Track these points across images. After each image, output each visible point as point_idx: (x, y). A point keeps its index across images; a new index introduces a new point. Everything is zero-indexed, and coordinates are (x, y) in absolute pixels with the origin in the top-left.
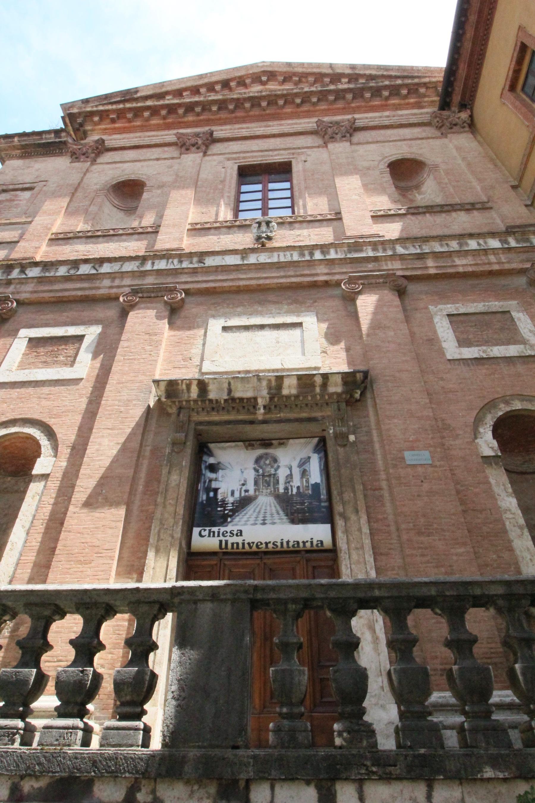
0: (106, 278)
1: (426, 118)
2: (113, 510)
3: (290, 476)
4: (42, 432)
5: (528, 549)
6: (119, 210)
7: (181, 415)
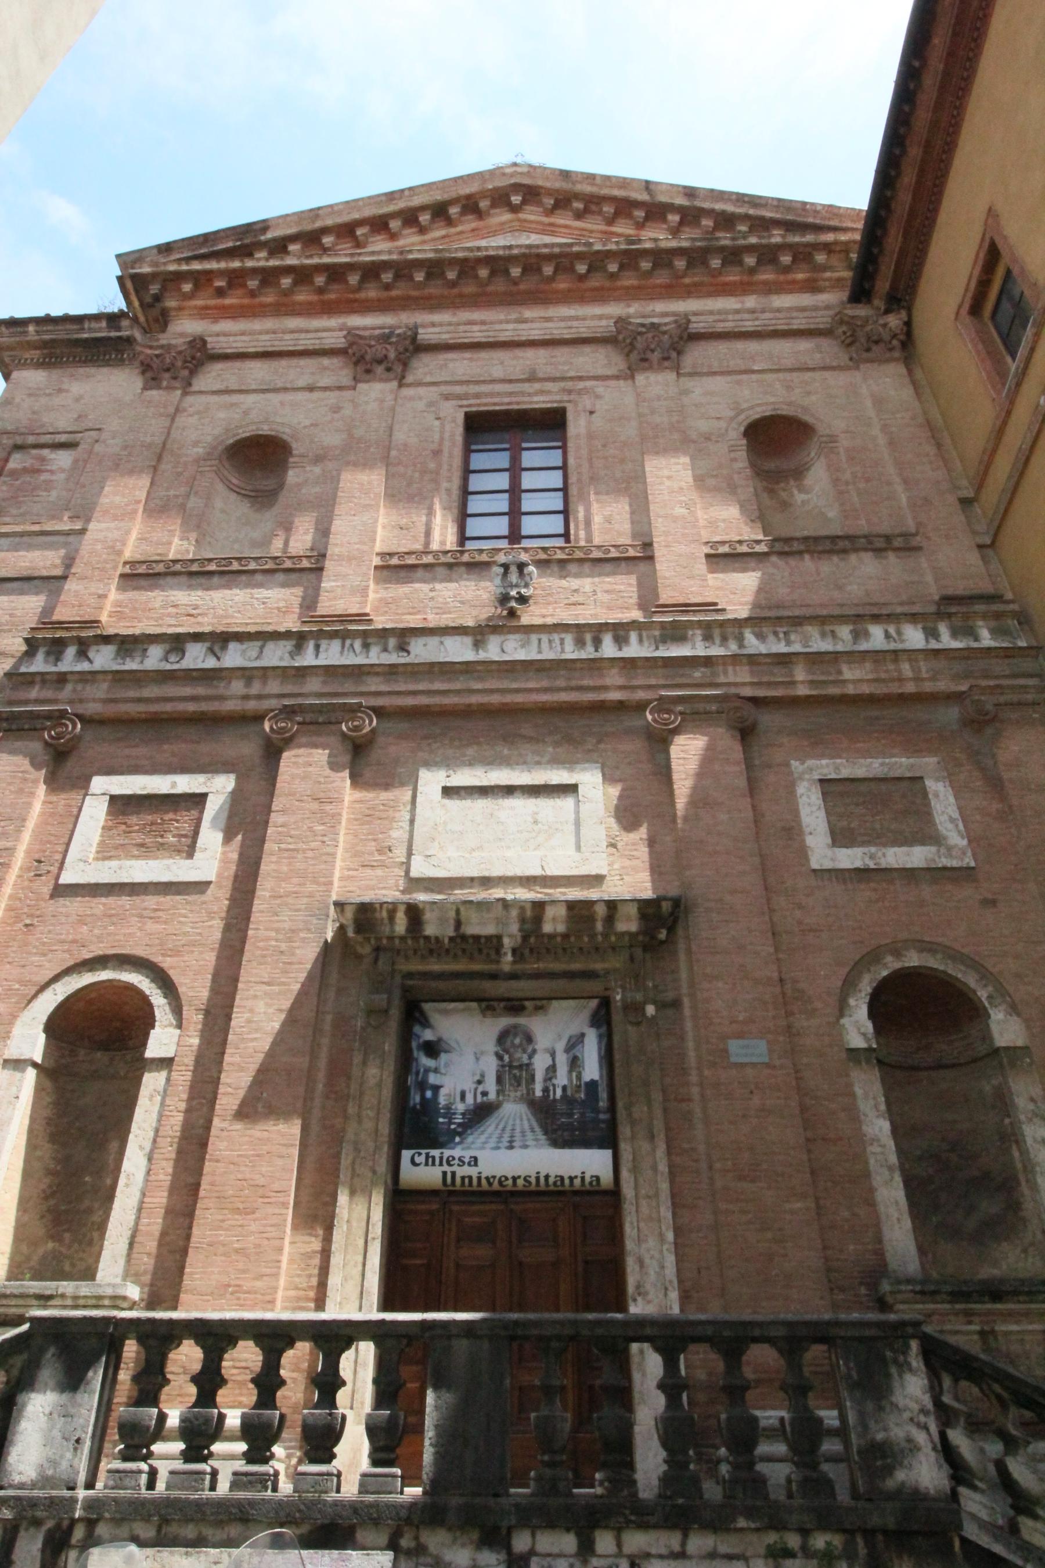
0: (237, 678)
1: (823, 320)
2: (282, 1127)
3: (552, 1069)
4: (152, 981)
5: (897, 1203)
6: (239, 498)
7: (380, 963)
